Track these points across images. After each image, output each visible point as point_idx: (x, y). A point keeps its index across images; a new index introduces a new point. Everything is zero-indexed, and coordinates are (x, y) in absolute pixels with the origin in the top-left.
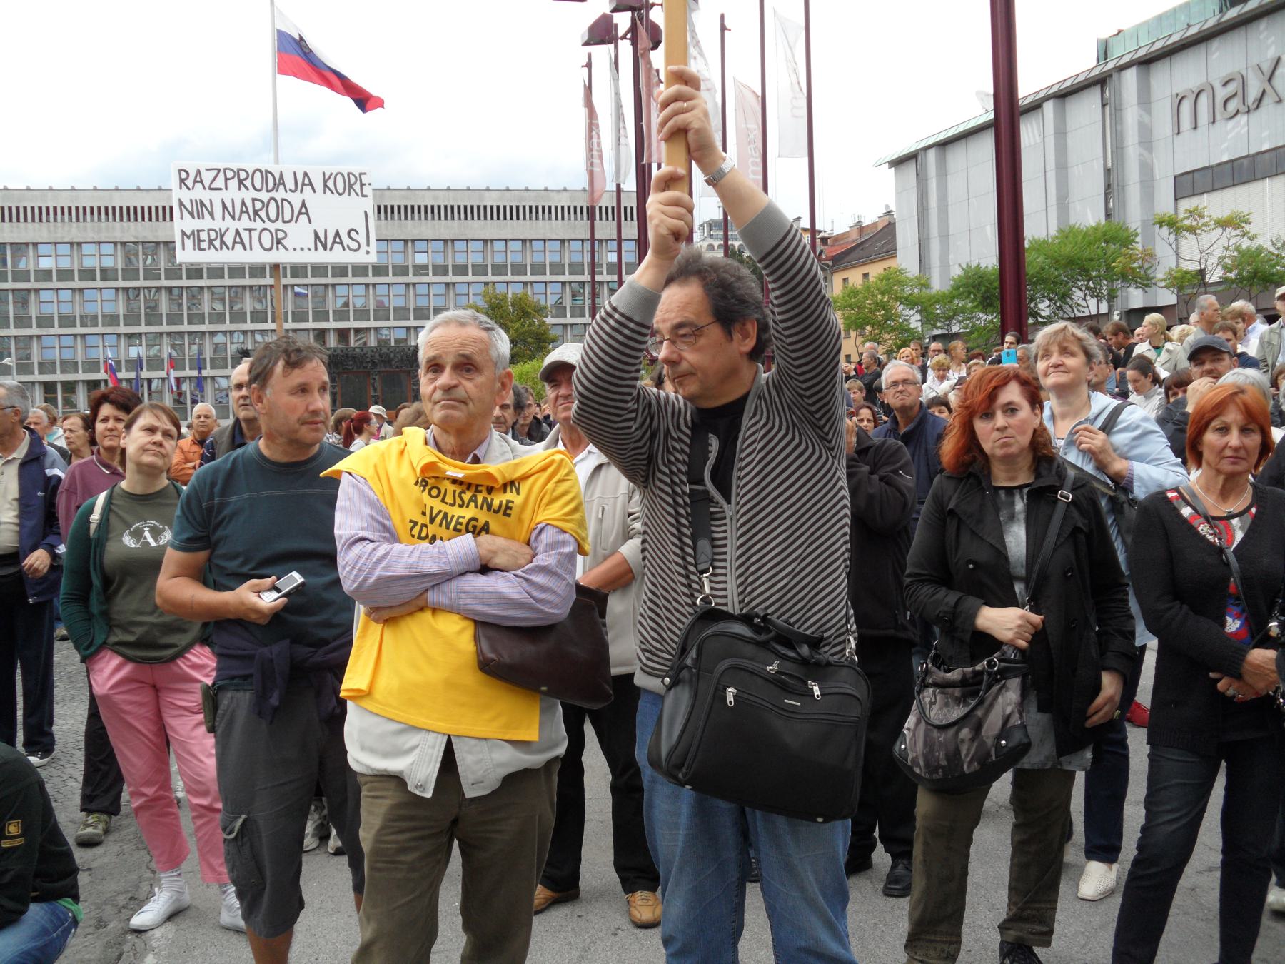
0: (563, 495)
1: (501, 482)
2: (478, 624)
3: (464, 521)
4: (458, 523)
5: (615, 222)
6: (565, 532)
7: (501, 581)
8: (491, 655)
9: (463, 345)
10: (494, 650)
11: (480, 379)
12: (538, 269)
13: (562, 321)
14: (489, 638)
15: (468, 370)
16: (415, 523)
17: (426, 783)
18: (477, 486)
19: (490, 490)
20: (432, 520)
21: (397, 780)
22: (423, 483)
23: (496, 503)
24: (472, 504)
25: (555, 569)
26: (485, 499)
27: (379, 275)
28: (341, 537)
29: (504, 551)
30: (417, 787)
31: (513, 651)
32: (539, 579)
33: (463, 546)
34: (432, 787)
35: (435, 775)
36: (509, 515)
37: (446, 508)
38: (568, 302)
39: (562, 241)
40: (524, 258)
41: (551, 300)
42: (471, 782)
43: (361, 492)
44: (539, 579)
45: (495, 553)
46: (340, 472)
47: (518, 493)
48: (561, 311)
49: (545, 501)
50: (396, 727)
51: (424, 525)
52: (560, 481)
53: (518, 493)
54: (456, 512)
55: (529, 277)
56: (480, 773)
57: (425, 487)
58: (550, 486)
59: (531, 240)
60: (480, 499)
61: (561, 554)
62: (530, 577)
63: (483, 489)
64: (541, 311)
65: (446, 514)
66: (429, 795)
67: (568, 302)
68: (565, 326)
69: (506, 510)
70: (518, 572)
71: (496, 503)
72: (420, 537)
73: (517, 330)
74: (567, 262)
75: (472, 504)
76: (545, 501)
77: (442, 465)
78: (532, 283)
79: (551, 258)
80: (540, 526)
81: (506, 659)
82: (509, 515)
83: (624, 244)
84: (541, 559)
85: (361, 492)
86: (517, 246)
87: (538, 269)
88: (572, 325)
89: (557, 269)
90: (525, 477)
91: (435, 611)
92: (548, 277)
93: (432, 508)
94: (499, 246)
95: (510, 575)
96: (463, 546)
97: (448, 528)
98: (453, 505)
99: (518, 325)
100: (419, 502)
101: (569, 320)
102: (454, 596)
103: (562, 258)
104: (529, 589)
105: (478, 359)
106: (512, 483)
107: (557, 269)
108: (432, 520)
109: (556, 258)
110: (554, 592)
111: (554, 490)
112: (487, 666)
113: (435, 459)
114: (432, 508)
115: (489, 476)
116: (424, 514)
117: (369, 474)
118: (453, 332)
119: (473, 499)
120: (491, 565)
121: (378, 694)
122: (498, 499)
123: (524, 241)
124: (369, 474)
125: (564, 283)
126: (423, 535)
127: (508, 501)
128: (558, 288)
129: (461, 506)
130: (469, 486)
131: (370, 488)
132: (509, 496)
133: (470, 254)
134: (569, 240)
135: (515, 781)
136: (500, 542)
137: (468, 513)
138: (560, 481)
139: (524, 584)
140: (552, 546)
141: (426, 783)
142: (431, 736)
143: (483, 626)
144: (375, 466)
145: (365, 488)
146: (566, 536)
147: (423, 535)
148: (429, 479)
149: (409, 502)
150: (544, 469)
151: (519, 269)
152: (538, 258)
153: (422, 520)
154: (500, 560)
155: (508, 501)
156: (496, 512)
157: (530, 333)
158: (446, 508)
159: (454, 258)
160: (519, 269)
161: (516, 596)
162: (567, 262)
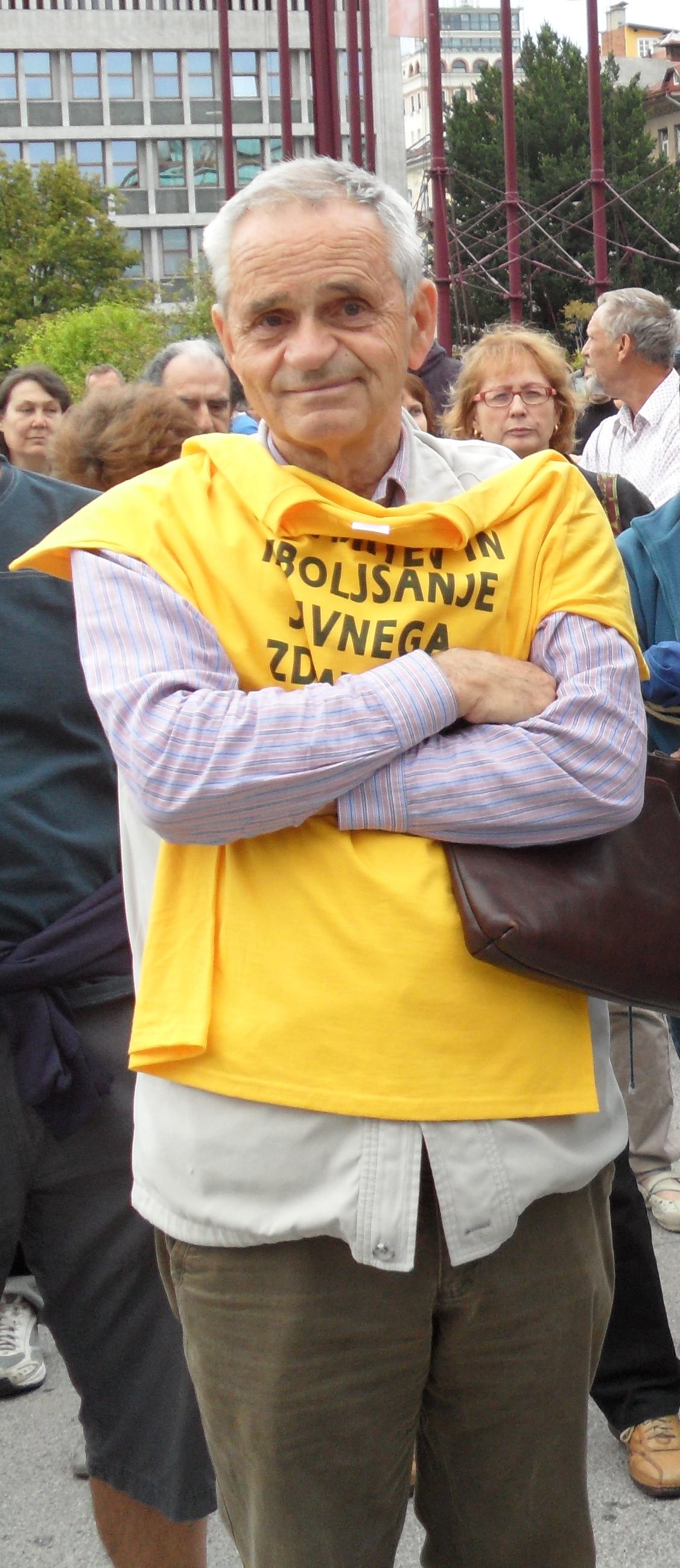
0: (586, 547)
1: (467, 534)
2: (451, 850)
3: (396, 632)
4: (381, 638)
5: (274, 14)
6: (605, 626)
7: (496, 744)
8: (501, 918)
9: (334, 259)
10: (502, 904)
11: (382, 326)
12: (86, 113)
13: (140, 221)
14: (485, 881)
15: (353, 311)
16: (282, 648)
17: (395, 1239)
18: (409, 552)
19: (438, 557)
20: (321, 637)
21: (321, 1254)
22: (283, 554)
23: (461, 585)
24: (409, 592)
25: (611, 702)
26: (434, 579)
27: (182, 115)
28: (107, 701)
29: (502, 681)
30: (376, 1252)
31: (533, 904)
32: (584, 729)
33: (414, 681)
34: (411, 1247)
35: (414, 1218)
36: (489, 608)
37: (347, 607)
38: (150, 180)
39: (136, 53)
40: (55, 88)
41: (114, 179)
42: (466, 1225)
43: (138, 589)
44: (584, 729)
45: (483, 686)
46: (65, 556)
47: (500, 555)
48: (137, 202)
49: (551, 565)
50: (308, 1125)
51: (302, 651)
52: (576, 518)
53: (500, 555)
54: (370, 613)
55: (66, 131)
56: (485, 1203)
57: (289, 561)
58: (557, 530)
59: (69, 52)
60: (423, 576)
61: (613, 672)
62: (565, 727)
63: (426, 557)
64: (98, 199)
65: (349, 622)
66: (406, 1264)
67: (150, 180)
68: (145, 232)
69: (481, 595)
70: (537, 721)
71: (461, 585)
72: (298, 679)
73: (53, 242)
74: (146, 98)
75: (409, 592)
76: (551, 565)
77: (332, 508)
78: (74, 142)
79: (113, 90)
80: (553, 620)
81: (534, 922)
82: (489, 608)
83: (236, 58)
84: (573, 689)
85: (138, 589)
86: (41, 64)
87: (86, 113)
88: (160, 230)
89: (127, 112)
90: (506, 521)
91: (356, 834)
92: (107, 130)
93: (317, 610)
94: (84, 63)
95: (518, 730)
96: (414, 681)
97: (360, 651)
98: (360, 598)
99: (53, 231)
100: (284, 597)
101: (153, 219)
102: (397, 799)
103: (136, 88)
104: (564, 754)
105: (370, 285)
106: (481, 537)
107: (127, 112)
108: (321, 637)
109: (123, 90)
110: (616, 757)
111: (566, 541)
112: (491, 947)
113: (315, 496)
114: (317, 610)
115: (442, 525)
116: (297, 624)
117: (147, 546)
118: (299, 227)
119: (409, 581)
120: (472, 719)
121: (230, 1053)
122: (461, 575)
123: (54, 54)
124: (147, 546)
125: (141, 143)
126: (305, 672)
127: (486, 576)
128: (129, 152)
129: (380, 599)
130: (391, 551)
131: (157, 576)
132: (483, 564)
133: (22, 80)
134: (150, 52)
135: (546, 1214)
136: (486, 663)
137: (404, 611)
138: (576, 518)
139: (551, 743)
140: (591, 658)
141: (395, 1239)
142: (386, 1137)
143: (466, 853)
144: (159, 528)
145: (149, 580)
146: (611, 634)
147: (305, 672)
148: (297, 546)
149: (259, 600)
150: (540, 495)
151: (45, 113)
152: (86, 91)
153: (292, 639)
154: (498, 701)
155: (486, 576)
156: (462, 603)
157: (82, 247)
158: (347, 607)
159: (72, 87)
160: (45, 113)
161: (521, 778)
162: (146, 98)
